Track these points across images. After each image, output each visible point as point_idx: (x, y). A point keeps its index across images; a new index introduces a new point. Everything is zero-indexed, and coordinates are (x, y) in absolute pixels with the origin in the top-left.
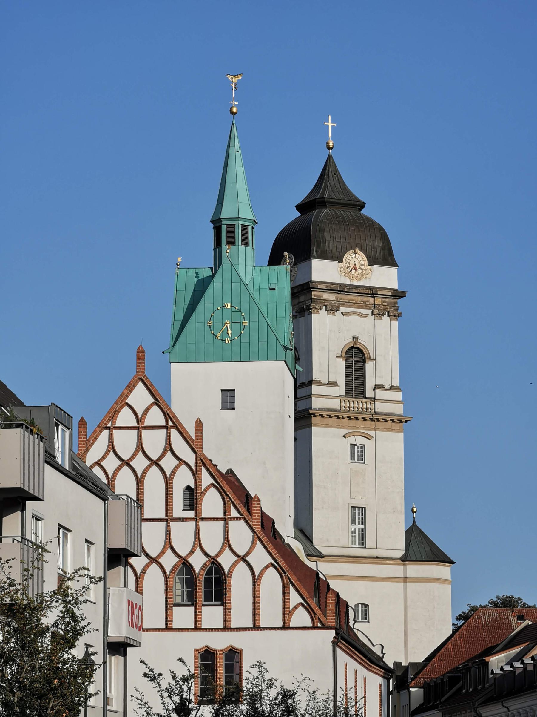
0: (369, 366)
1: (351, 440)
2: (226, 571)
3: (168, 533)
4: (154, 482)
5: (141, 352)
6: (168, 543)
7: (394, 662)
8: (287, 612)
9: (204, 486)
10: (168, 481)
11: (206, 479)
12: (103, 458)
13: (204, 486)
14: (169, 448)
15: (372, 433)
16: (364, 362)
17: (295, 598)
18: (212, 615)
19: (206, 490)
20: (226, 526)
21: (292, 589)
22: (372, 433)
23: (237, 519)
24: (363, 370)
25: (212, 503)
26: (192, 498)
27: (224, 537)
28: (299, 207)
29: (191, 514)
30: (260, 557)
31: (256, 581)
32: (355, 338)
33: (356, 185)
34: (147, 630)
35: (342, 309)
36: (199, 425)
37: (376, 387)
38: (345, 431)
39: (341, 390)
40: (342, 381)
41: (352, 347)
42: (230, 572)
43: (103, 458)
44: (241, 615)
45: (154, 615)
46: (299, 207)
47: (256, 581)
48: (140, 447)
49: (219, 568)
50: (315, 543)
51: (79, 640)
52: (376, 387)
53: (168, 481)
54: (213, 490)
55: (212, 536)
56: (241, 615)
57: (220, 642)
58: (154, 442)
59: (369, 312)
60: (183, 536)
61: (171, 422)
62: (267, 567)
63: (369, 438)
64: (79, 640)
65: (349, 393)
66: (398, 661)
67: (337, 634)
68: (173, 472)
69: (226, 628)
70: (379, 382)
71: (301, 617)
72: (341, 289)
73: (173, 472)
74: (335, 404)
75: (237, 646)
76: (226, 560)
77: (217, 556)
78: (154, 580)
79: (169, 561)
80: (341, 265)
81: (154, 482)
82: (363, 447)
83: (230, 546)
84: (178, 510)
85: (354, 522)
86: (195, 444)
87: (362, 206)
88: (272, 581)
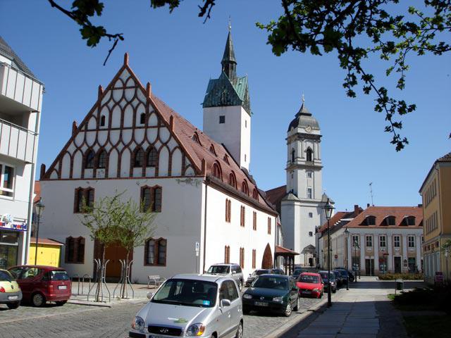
5: (126, 56)
6: (133, 139)
7: (375, 217)
8: (184, 168)
9: (150, 112)
10: (135, 111)
18: (150, 171)
19: (150, 115)
21: (97, 109)
25: (153, 120)
26: (144, 118)
29: (143, 125)
31: (171, 154)
32: (267, 43)
36: (148, 85)
39: (306, 160)
40: (305, 157)
47: (171, 154)
51: (83, 38)
53: (135, 111)
56: (163, 168)
57: (152, 183)
58: (130, 94)
61: (137, 85)
62: (175, 148)
64: (83, 38)
65: (307, 160)
66: (278, 57)
69: (157, 176)
74: (304, 163)
75: (160, 185)
76: (158, 145)
78: (127, 156)
79: (133, 146)
84: (138, 123)
86: (146, 93)
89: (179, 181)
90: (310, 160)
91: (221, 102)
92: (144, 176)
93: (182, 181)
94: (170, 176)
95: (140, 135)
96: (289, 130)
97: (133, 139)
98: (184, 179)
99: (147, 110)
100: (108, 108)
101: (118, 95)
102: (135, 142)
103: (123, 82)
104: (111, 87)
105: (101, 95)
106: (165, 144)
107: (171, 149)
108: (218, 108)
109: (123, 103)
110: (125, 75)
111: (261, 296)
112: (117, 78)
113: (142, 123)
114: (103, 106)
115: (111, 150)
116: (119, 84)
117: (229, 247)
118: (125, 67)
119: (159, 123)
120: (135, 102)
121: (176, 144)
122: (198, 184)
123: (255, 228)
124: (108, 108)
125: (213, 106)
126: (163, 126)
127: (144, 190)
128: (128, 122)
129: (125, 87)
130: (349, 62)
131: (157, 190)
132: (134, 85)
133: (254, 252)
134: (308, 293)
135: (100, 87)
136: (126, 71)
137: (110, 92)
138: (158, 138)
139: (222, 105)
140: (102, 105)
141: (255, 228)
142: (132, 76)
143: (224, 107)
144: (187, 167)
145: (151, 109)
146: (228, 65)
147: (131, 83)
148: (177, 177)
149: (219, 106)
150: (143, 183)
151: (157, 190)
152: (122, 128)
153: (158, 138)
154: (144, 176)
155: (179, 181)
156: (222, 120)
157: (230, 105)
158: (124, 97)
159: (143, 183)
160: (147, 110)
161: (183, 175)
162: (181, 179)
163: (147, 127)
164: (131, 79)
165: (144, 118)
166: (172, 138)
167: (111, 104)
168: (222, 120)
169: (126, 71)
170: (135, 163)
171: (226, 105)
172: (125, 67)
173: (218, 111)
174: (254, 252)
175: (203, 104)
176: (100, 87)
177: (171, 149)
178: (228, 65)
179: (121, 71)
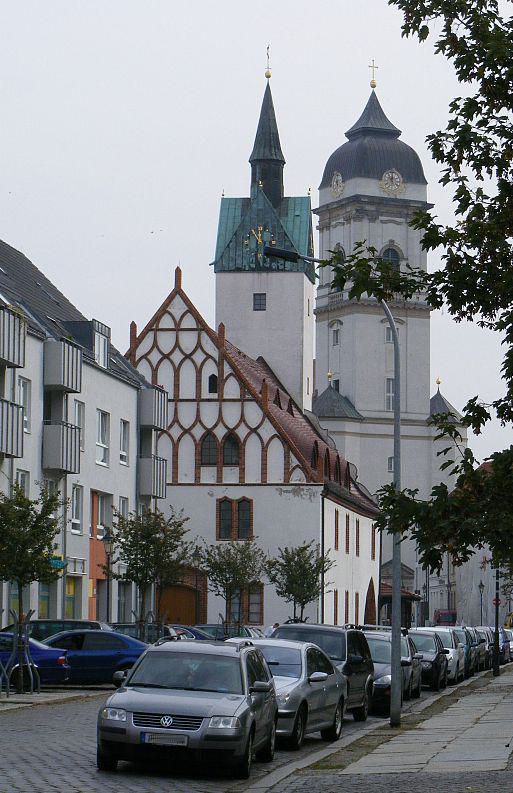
2: (242, 440)
3: (198, 411)
4: (188, 373)
5: (178, 272)
6: (198, 419)
8: (288, 473)
11: (227, 370)
12: (149, 352)
14: (199, 345)
17: (294, 462)
18: (231, 475)
21: (292, 456)
22: (404, 319)
23: (251, 400)
25: (232, 389)
26: (215, 384)
27: (234, 414)
28: (348, 135)
29: (215, 396)
30: (267, 431)
31: (264, 449)
42: (245, 441)
43: (149, 352)
45: (186, 473)
46: (348, 135)
47: (264, 449)
48: (177, 345)
49: (237, 438)
50: (357, 408)
54: (232, 379)
55: (231, 415)
56: (253, 474)
57: (235, 494)
58: (188, 341)
59: (402, 220)
62: (272, 438)
67: (325, 489)
69: (242, 483)
71: (298, 476)
76: (242, 432)
77: (235, 428)
78: (187, 450)
79: (198, 432)
81: (188, 373)
83: (244, 421)
84: (206, 394)
85: (389, 391)
87: (398, 133)
88: (277, 450)
91: (257, 262)
92: (219, 483)
93: (286, 491)
94: (264, 483)
96: (326, 182)
97: (198, 419)
98: (290, 488)
99: (221, 371)
101: (166, 342)
103: (174, 318)
104: (153, 326)
105: (136, 341)
107: (266, 438)
108: (249, 276)
109: (177, 357)
110: (177, 308)
112: (164, 310)
114: (140, 359)
116: (166, 322)
118: (178, 291)
119: (243, 394)
120: (199, 357)
121: (274, 432)
123: (358, 554)
125: (239, 270)
127: (224, 505)
128: (188, 390)
129: (177, 329)
130: (502, 132)
131: (246, 503)
135: (133, 326)
136: (178, 298)
137: (151, 335)
138: (242, 419)
139: (259, 269)
141: (358, 554)
143: (264, 275)
147: (189, 322)
148: (277, 485)
149: (252, 270)
150: (221, 492)
151: (246, 503)
153: (242, 419)
156: (260, 301)
161: (286, 483)
162: (284, 488)
163: (221, 400)
165: (215, 384)
167: (155, 357)
168: (260, 301)
169: (178, 298)
170: (202, 461)
172: (178, 291)
173: (249, 282)
175: (215, 263)
176: (133, 326)
177: (266, 438)
179: (171, 298)
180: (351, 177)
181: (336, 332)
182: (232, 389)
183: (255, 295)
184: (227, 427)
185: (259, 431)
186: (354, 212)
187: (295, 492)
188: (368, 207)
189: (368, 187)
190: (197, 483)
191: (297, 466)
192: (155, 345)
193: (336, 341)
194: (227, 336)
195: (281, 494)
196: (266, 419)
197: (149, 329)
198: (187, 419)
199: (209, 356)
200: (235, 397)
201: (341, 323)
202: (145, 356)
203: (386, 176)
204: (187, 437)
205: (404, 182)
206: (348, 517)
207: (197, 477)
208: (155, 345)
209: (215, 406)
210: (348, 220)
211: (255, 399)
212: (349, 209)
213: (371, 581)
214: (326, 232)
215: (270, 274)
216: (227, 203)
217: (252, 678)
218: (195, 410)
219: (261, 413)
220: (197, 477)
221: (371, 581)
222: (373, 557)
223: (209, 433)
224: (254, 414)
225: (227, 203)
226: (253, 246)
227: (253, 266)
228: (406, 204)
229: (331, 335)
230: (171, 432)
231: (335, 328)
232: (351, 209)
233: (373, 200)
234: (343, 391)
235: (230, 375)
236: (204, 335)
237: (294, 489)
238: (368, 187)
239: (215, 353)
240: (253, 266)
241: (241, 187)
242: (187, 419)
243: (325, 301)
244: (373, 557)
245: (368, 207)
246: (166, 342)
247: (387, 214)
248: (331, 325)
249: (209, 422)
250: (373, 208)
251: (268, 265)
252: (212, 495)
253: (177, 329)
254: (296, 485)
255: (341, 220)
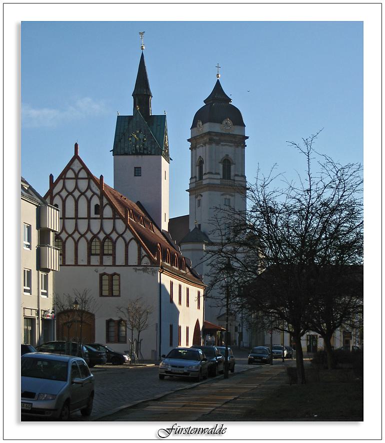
0: (232, 167)
1: (224, 197)
4: (83, 203)
5: (76, 145)
8: (140, 259)
9: (104, 204)
11: (105, 201)
13: (104, 204)
15: (233, 194)
16: (230, 165)
17: (144, 253)
19: (105, 206)
20: (114, 222)
24: (230, 168)
25: (108, 212)
26: (99, 209)
28: (205, 101)
29: (98, 216)
31: (127, 245)
33: (227, 91)
34: (130, 266)
35: (222, 143)
37: (236, 175)
38: (222, 193)
40: (221, 172)
41: (226, 159)
44: (120, 260)
46: (205, 101)
47: (127, 245)
52: (236, 175)
56: (120, 260)
57: (110, 271)
58: (83, 185)
60: (95, 226)
61: (90, 176)
63: (232, 196)
65: (224, 177)
68: (91, 198)
69: (114, 265)
70: (237, 173)
72: (222, 134)
73: (91, 198)
74: (218, 182)
76: (114, 236)
78: (83, 246)
79: (89, 236)
80: (221, 125)
81: (83, 203)
82: (229, 199)
83: (115, 230)
84: (93, 215)
88: (133, 246)
89: (136, 270)
90: (229, 178)
92: (101, 264)
93: (139, 270)
94: (127, 265)
95: (95, 226)
96: (194, 125)
99: (102, 202)
100: (61, 197)
102: (91, 232)
103: (74, 172)
104: (63, 176)
105: (53, 185)
106: (121, 235)
107: (128, 239)
108: (132, 157)
110: (76, 166)
111: (168, 380)
112: (68, 167)
113: (96, 214)
115: (67, 239)
116: (70, 174)
117: (172, 325)
118: (76, 157)
119: (114, 215)
120: (89, 194)
122: (155, 272)
123: (188, 305)
124: (61, 197)
125: (126, 154)
126: (118, 218)
128: (83, 212)
129: (77, 178)
132: (86, 177)
133: (187, 328)
134: (259, 360)
135: (51, 177)
136: (76, 161)
137: (61, 181)
138: (114, 229)
139: (137, 153)
140: (54, 194)
141: (188, 305)
142: (84, 167)
143: (140, 156)
144: (143, 257)
145: (105, 201)
146: (142, 94)
147: (83, 174)
150: (101, 270)
152: (76, 218)
153: (114, 229)
154: (101, 264)
155: (136, 270)
156: (138, 171)
157: (148, 154)
158: (77, 187)
159: (101, 270)
160: (102, 202)
161: (139, 264)
162: (138, 268)
163: (102, 218)
164: (83, 170)
165: (99, 209)
166: (128, 229)
167: (64, 194)
168: (138, 171)
169: (76, 161)
171: (143, 154)
172: (76, 157)
173: (132, 161)
174: (187, 328)
176: (51, 177)
178: (142, 94)
180: (206, 123)
181: (199, 201)
182: (108, 212)
183: (135, 168)
184: (105, 233)
185: (124, 235)
186: (208, 140)
187: (144, 270)
188: (215, 138)
189: (217, 128)
190: (89, 264)
191: (145, 256)
192: (64, 187)
193: (199, 205)
194: (104, 181)
195: (136, 271)
196: (128, 229)
197: (60, 178)
198: (83, 228)
199: (94, 194)
200: (109, 217)
201: (202, 196)
202: (58, 194)
203: (224, 122)
204: (83, 239)
205: (233, 125)
206: (180, 286)
207: (89, 261)
208: (64, 187)
209: (98, 222)
210: (205, 144)
211: (121, 217)
212: (205, 139)
213: (198, 321)
214: (194, 151)
215: (143, 156)
216: (120, 119)
217: (165, 357)
218: (87, 224)
219: (124, 226)
220: (89, 261)
221: (198, 321)
222: (199, 308)
223: (95, 236)
224: (120, 226)
225: (120, 119)
226: (134, 141)
227: (134, 152)
228: (234, 136)
229: (197, 202)
230: (87, 236)
231: (198, 198)
232: (206, 139)
233: (217, 134)
234: (202, 230)
235: (107, 204)
236: (92, 182)
237: (143, 268)
238: (217, 128)
239: (98, 192)
240: (134, 152)
241: (128, 110)
242: (83, 228)
243: (194, 185)
244: (199, 308)
245: (215, 138)
246: (70, 185)
247: (225, 141)
248: (196, 197)
249: (108, 231)
250: (217, 138)
251: (142, 152)
252: (97, 272)
253: (77, 178)
254: (144, 266)
255: (202, 145)
